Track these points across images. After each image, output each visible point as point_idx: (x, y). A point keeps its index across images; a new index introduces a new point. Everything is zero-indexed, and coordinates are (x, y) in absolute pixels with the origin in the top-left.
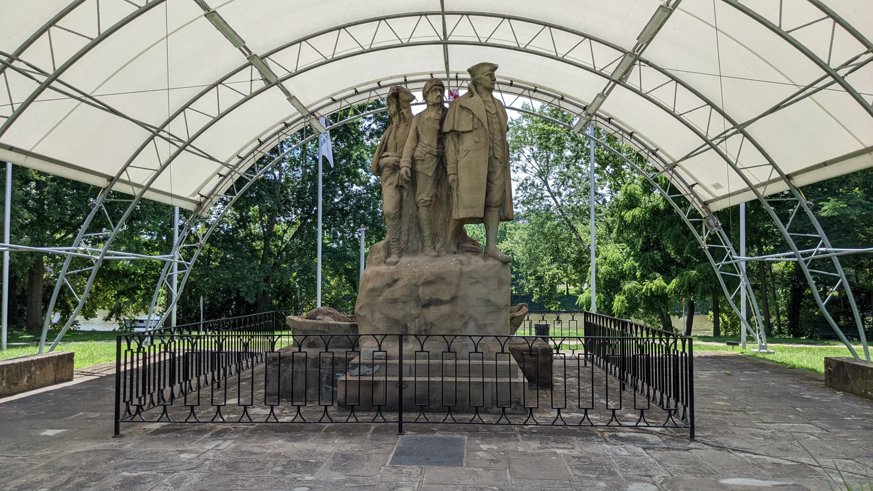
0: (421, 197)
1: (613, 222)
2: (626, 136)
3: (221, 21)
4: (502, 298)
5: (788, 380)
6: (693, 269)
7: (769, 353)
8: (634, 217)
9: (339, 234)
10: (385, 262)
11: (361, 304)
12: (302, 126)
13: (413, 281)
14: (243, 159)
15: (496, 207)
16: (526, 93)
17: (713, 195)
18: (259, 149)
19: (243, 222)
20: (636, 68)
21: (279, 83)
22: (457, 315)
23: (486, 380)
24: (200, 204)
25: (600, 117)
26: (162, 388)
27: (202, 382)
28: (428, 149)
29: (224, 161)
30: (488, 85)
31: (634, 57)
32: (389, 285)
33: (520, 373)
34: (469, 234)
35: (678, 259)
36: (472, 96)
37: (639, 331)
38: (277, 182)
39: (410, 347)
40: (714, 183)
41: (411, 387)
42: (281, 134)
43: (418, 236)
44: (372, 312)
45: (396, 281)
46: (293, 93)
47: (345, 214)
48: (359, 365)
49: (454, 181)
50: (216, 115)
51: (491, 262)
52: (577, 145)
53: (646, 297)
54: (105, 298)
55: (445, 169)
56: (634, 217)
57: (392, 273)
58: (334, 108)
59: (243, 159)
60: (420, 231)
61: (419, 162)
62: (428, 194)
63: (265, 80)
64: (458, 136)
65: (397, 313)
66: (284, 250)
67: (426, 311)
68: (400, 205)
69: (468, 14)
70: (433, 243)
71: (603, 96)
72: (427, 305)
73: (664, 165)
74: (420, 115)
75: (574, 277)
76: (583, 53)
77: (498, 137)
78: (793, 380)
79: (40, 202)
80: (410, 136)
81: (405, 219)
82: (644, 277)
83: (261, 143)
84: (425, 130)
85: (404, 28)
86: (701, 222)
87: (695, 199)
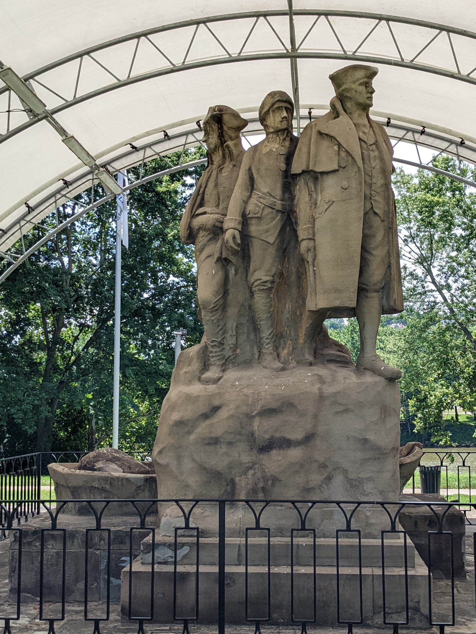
4: (388, 436)
9: (150, 342)
10: (199, 379)
11: (161, 446)
12: (89, 185)
13: (245, 409)
15: (377, 289)
16: (409, 136)
18: (28, 218)
21: (48, 116)
22: (315, 465)
23: (366, 571)
28: (268, 200)
30: (362, 99)
32: (206, 416)
33: (419, 560)
38: (62, 271)
39: (238, 517)
42: (58, 196)
43: (252, 337)
44: (179, 458)
45: (216, 409)
46: (70, 132)
47: (157, 314)
51: (369, 379)
55: (295, 231)
57: (212, 396)
58: (135, 158)
62: (269, 271)
63: (29, 111)
65: (219, 460)
66: (74, 363)
67: (264, 458)
68: (224, 289)
69: (327, 14)
70: (276, 348)
72: (267, 447)
74: (255, 148)
77: (378, 181)
81: (232, 311)
83: (31, 209)
84: (263, 168)
85: (233, 36)
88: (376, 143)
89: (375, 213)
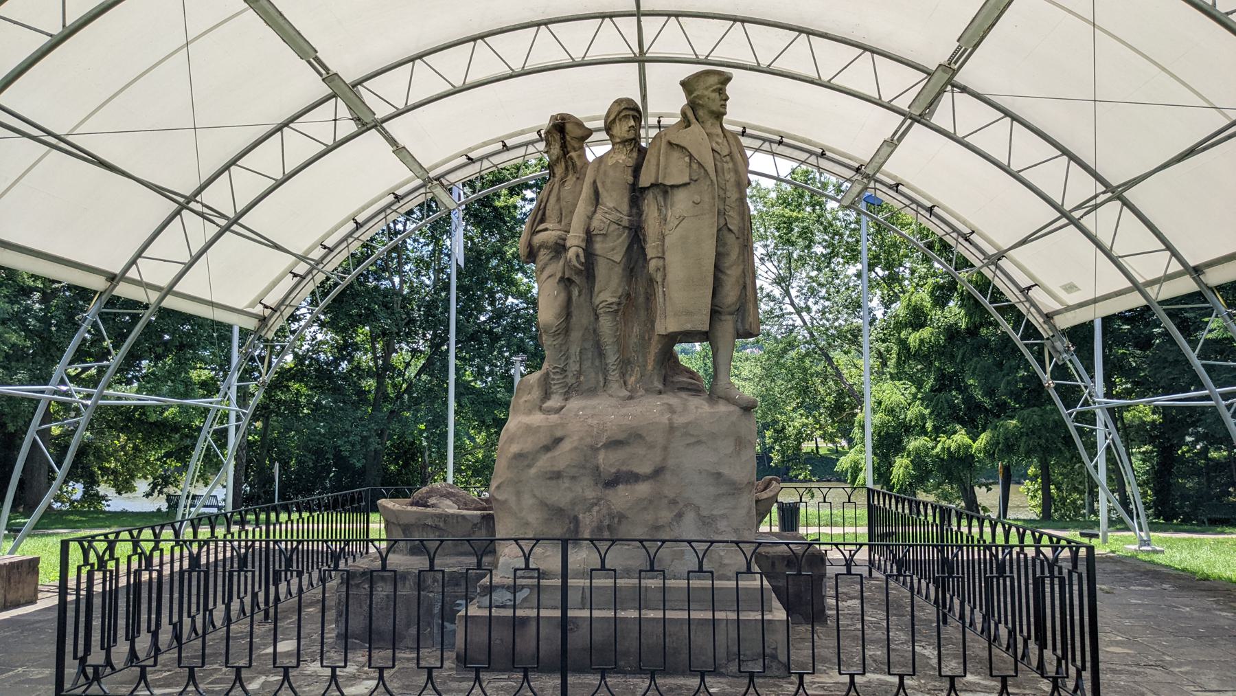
0: (602, 297)
1: (888, 351)
2: (923, 212)
3: (271, 10)
4: (743, 469)
5: (1208, 602)
6: (1012, 418)
7: (1156, 552)
8: (922, 341)
9: (487, 368)
10: (540, 409)
11: (500, 481)
12: (421, 199)
14: (331, 250)
16: (766, 146)
17: (1061, 303)
18: (356, 235)
19: (345, 350)
20: (947, 97)
21: (378, 125)
24: (263, 320)
25: (881, 182)
26: (211, 607)
27: (234, 615)
28: (614, 216)
29: (299, 253)
30: (714, 108)
31: (944, 79)
32: (547, 448)
34: (682, 358)
35: (987, 403)
36: (689, 125)
37: (930, 512)
39: (581, 557)
40: (1067, 281)
41: (585, 626)
42: (389, 211)
43: (597, 363)
44: (518, 494)
46: (401, 142)
47: (495, 338)
48: (491, 589)
49: (658, 269)
50: (279, 176)
51: (722, 408)
52: (833, 238)
53: (942, 460)
54: (148, 462)
55: (643, 249)
56: (922, 341)
57: (553, 427)
59: (331, 250)
60: (601, 355)
61: (598, 239)
62: (615, 292)
64: (665, 193)
65: (561, 495)
67: (610, 493)
68: (567, 311)
70: (623, 375)
71: (892, 143)
72: (613, 482)
73: (982, 257)
75: (830, 430)
76: (860, 75)
77: (733, 195)
78: (1217, 602)
79: (45, 320)
80: (583, 195)
81: (576, 335)
82: (937, 430)
83: (359, 226)
84: (608, 181)
85: (576, 38)
86: (1042, 347)
87: (1032, 310)
88: (730, 154)
89: (730, 230)
